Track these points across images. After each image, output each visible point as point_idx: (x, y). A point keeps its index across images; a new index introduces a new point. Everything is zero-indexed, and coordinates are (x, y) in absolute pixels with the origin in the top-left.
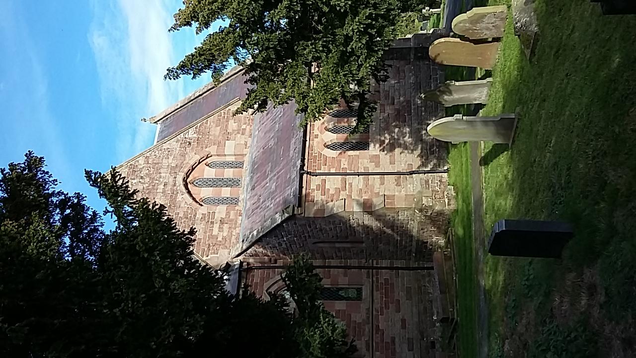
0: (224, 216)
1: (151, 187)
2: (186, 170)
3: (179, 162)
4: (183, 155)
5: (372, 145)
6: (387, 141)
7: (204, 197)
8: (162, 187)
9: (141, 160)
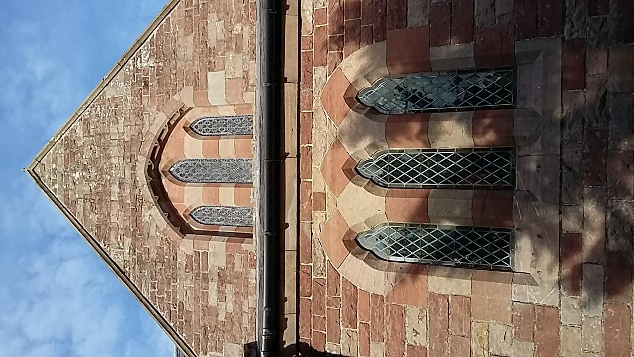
0: (223, 264)
1: (100, 189)
2: (147, 149)
3: (134, 131)
4: (139, 114)
5: (524, 247)
6: (591, 239)
7: (190, 207)
8: (115, 188)
9: (79, 126)
